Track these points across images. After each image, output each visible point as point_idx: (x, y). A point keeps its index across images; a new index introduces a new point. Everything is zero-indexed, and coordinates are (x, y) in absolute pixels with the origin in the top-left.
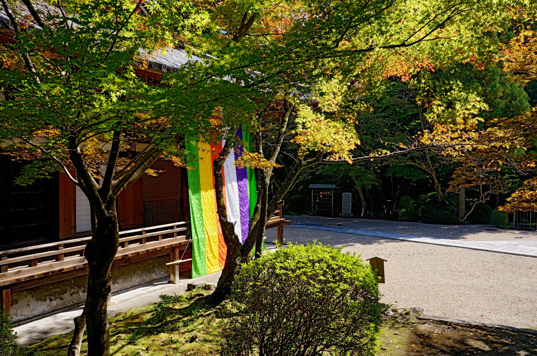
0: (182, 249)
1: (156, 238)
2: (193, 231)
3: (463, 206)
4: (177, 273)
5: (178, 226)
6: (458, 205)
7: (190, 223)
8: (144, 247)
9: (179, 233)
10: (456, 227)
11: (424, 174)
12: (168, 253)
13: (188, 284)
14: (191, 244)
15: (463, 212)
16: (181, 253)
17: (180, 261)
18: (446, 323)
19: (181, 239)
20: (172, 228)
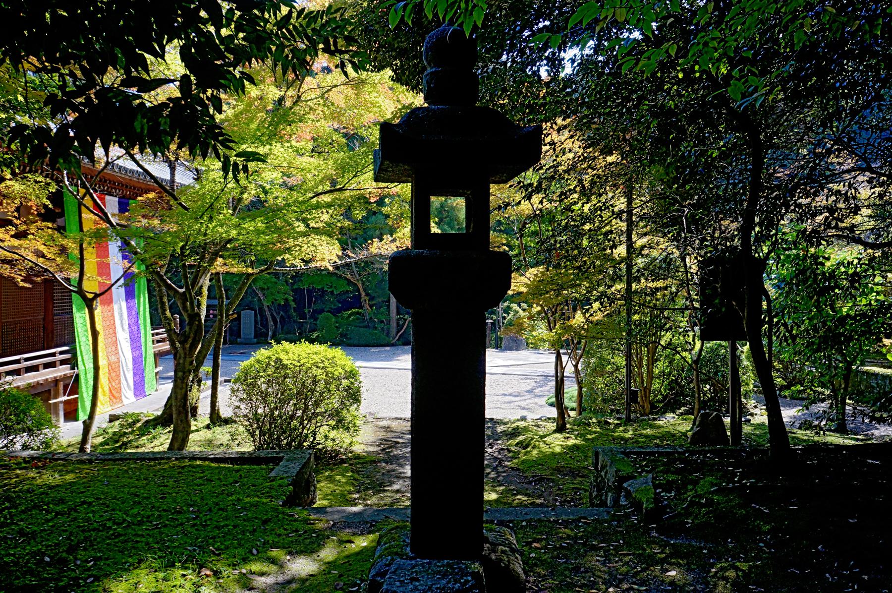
0: (67, 382)
1: (35, 368)
2: (79, 359)
3: (394, 324)
4: (62, 413)
5: (61, 353)
6: (389, 323)
7: (75, 349)
8: (23, 379)
9: (63, 362)
10: (388, 348)
11: (348, 284)
12: (44, 392)
13: (110, 416)
14: (77, 376)
15: (394, 331)
16: (66, 387)
17: (66, 398)
18: (401, 419)
19: (64, 370)
20: (53, 355)
